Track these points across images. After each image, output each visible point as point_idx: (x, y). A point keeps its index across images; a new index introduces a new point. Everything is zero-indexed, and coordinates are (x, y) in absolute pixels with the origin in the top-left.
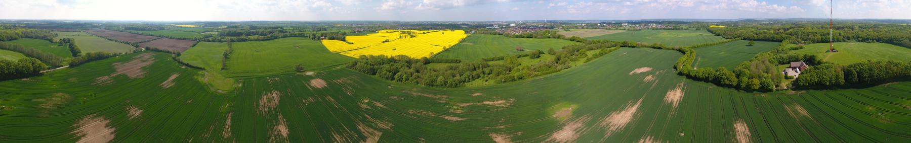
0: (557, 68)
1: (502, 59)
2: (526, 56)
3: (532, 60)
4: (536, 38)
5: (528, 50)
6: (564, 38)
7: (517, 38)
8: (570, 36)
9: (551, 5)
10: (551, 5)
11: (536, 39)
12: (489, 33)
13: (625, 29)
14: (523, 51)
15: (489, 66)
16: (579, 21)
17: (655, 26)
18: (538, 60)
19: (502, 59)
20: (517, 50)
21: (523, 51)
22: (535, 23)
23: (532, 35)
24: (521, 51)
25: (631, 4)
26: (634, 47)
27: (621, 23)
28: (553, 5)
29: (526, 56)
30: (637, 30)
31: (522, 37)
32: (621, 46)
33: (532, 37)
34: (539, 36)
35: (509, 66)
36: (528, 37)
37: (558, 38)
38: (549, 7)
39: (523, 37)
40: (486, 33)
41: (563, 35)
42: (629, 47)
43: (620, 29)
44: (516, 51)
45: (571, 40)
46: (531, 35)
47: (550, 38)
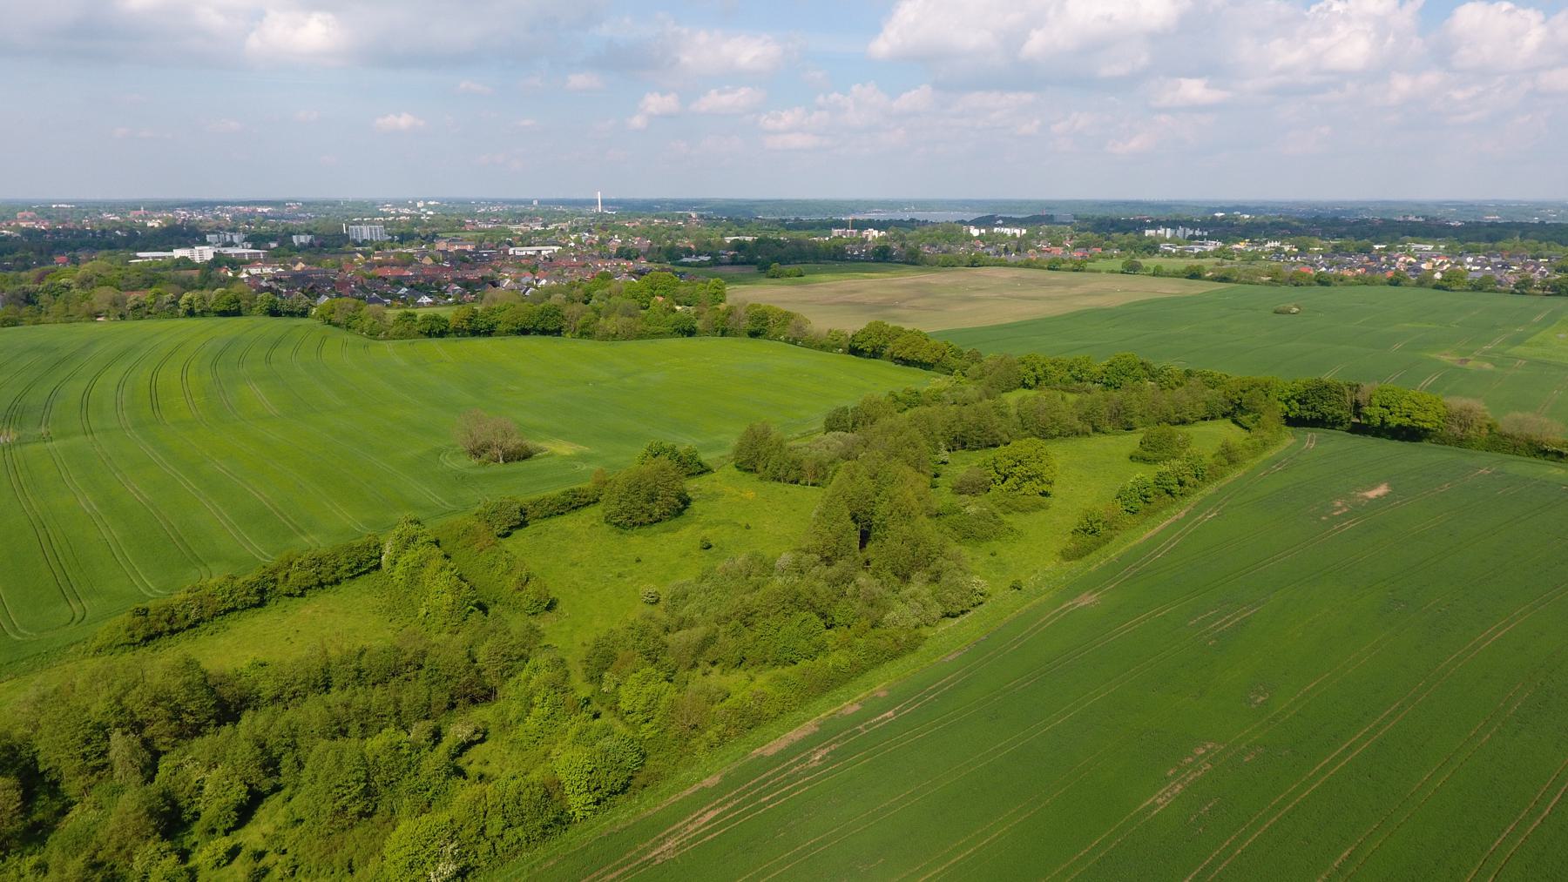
0: (679, 288)
1: (365, 564)
2: (574, 503)
3: (637, 542)
4: (586, 333)
5: (565, 449)
6: (800, 340)
7: (435, 344)
8: (852, 325)
9: (655, 102)
10: (655, 102)
11: (585, 346)
12: (172, 310)
13: (1194, 275)
14: (526, 455)
15: (228, 711)
16: (838, 206)
17: (1434, 260)
18: (685, 535)
19: (365, 564)
20: (476, 452)
21: (526, 455)
22: (532, 217)
23: (556, 312)
24: (509, 458)
25: (1214, 96)
26: (1411, 434)
27: (1140, 226)
28: (669, 102)
29: (574, 503)
30: (1296, 281)
31: (475, 333)
32: (1293, 422)
33: (558, 332)
34: (611, 324)
35: (448, 646)
36: (524, 332)
37: (754, 334)
38: (638, 121)
39: (489, 332)
40: (140, 312)
41: (788, 316)
42: (1358, 429)
43: (1158, 273)
44: (465, 464)
45: (855, 351)
46: (544, 314)
47: (691, 333)
